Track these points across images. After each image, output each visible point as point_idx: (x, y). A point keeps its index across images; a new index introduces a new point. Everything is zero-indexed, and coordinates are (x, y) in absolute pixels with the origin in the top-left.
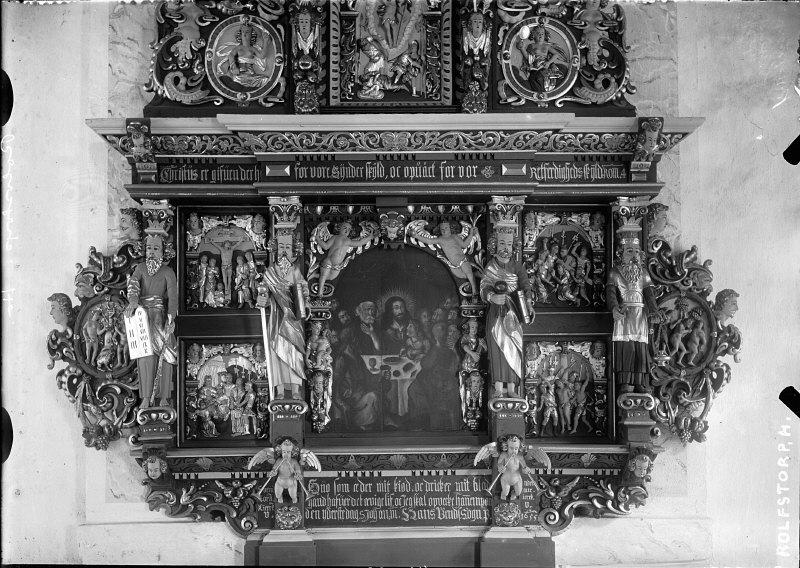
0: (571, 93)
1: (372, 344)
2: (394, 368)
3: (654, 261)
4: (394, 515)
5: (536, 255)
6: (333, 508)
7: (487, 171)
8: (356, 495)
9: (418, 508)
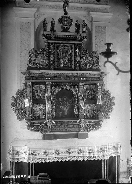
0: (91, 67)
2: (65, 108)
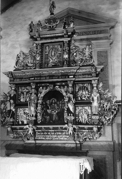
0: (83, 63)
1: (49, 108)
2: (53, 112)
4: (51, 139)
5: (78, 91)
6: (40, 137)
7: (67, 77)
8: (44, 135)
9: (55, 138)
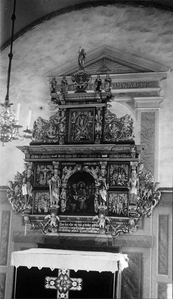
2: (80, 199)
3: (140, 176)
5: (113, 174)
8: (70, 226)
